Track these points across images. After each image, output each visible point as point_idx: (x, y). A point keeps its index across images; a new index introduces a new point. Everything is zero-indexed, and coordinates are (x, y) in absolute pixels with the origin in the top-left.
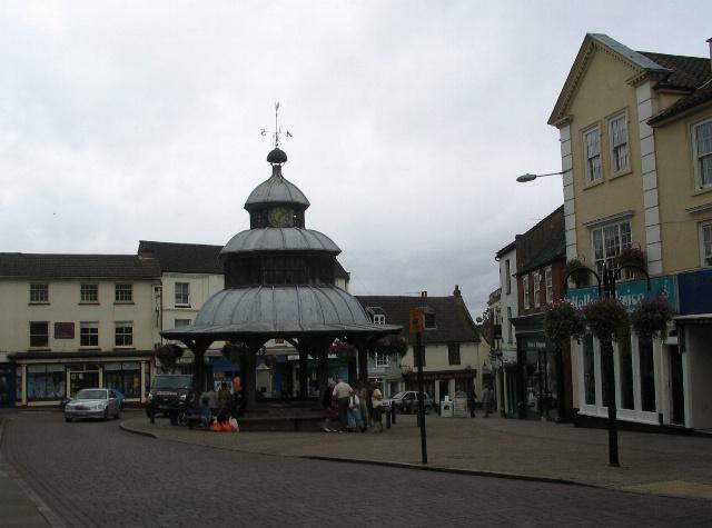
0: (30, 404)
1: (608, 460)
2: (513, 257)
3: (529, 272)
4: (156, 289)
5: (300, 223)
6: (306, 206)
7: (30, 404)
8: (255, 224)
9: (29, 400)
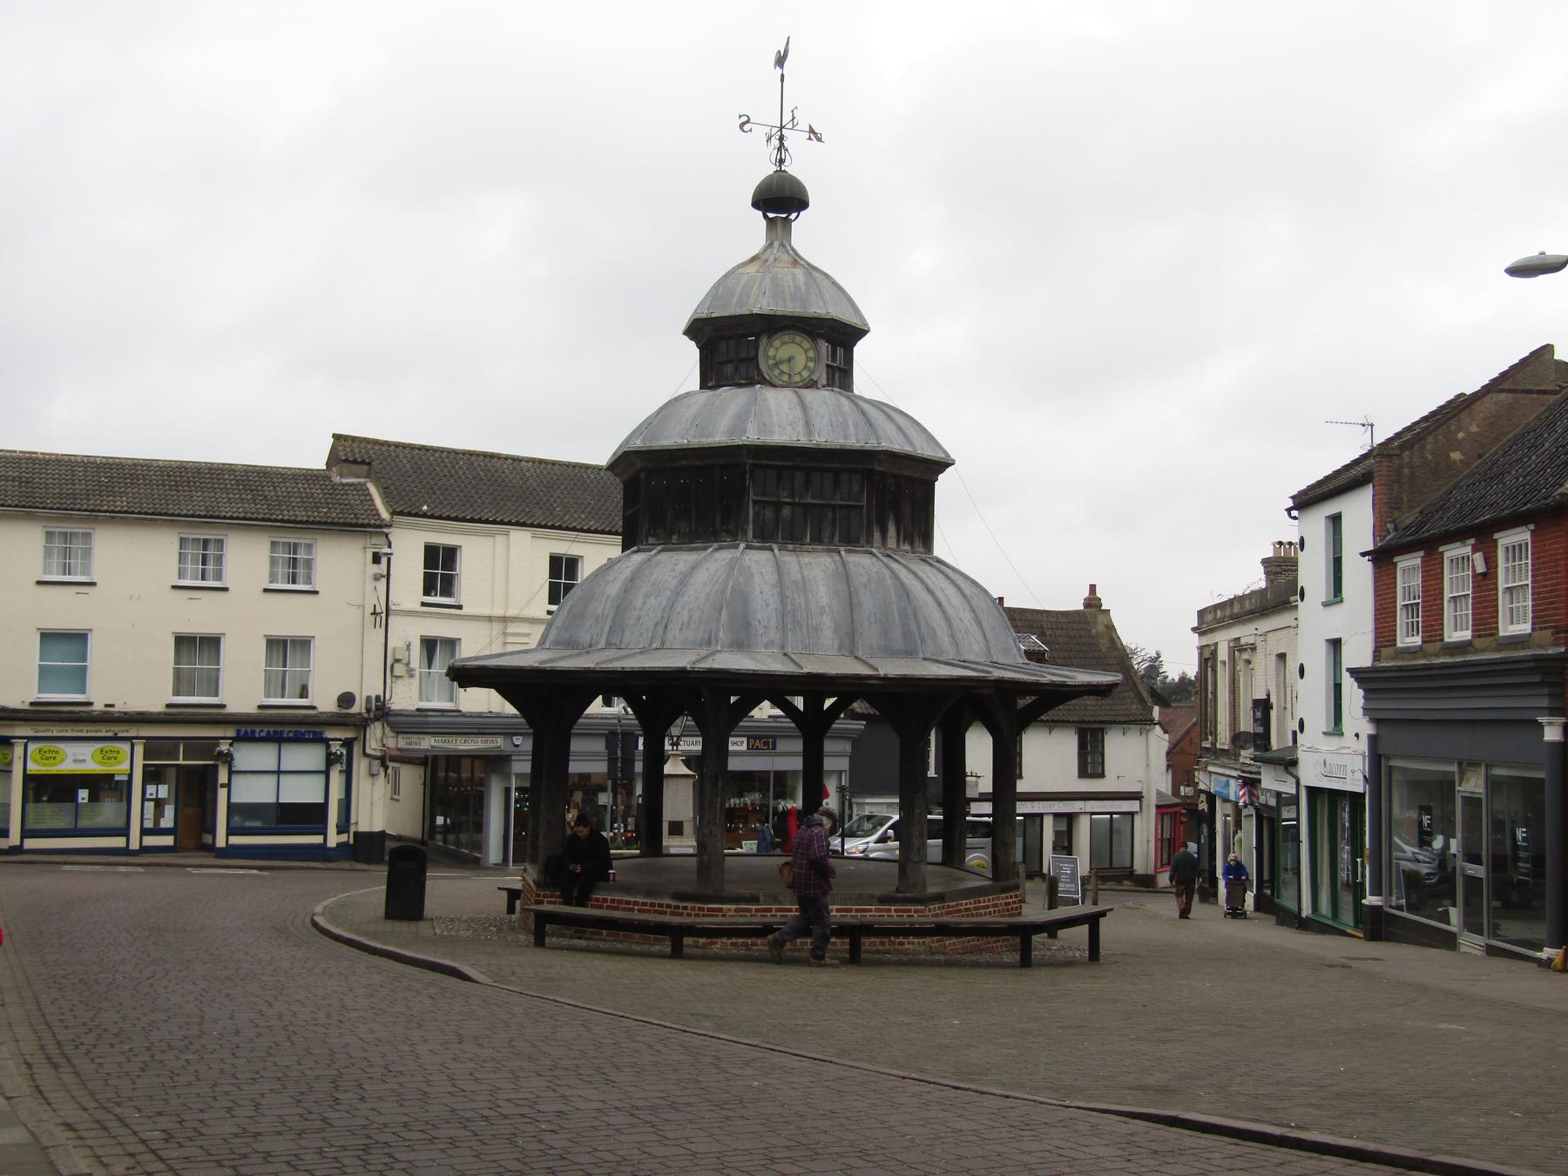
0: (30, 843)
1: (506, 909)
2: (1359, 512)
3: (1429, 546)
4: (376, 559)
5: (841, 375)
6: (857, 333)
7: (30, 843)
8: (712, 375)
9: (145, 832)
